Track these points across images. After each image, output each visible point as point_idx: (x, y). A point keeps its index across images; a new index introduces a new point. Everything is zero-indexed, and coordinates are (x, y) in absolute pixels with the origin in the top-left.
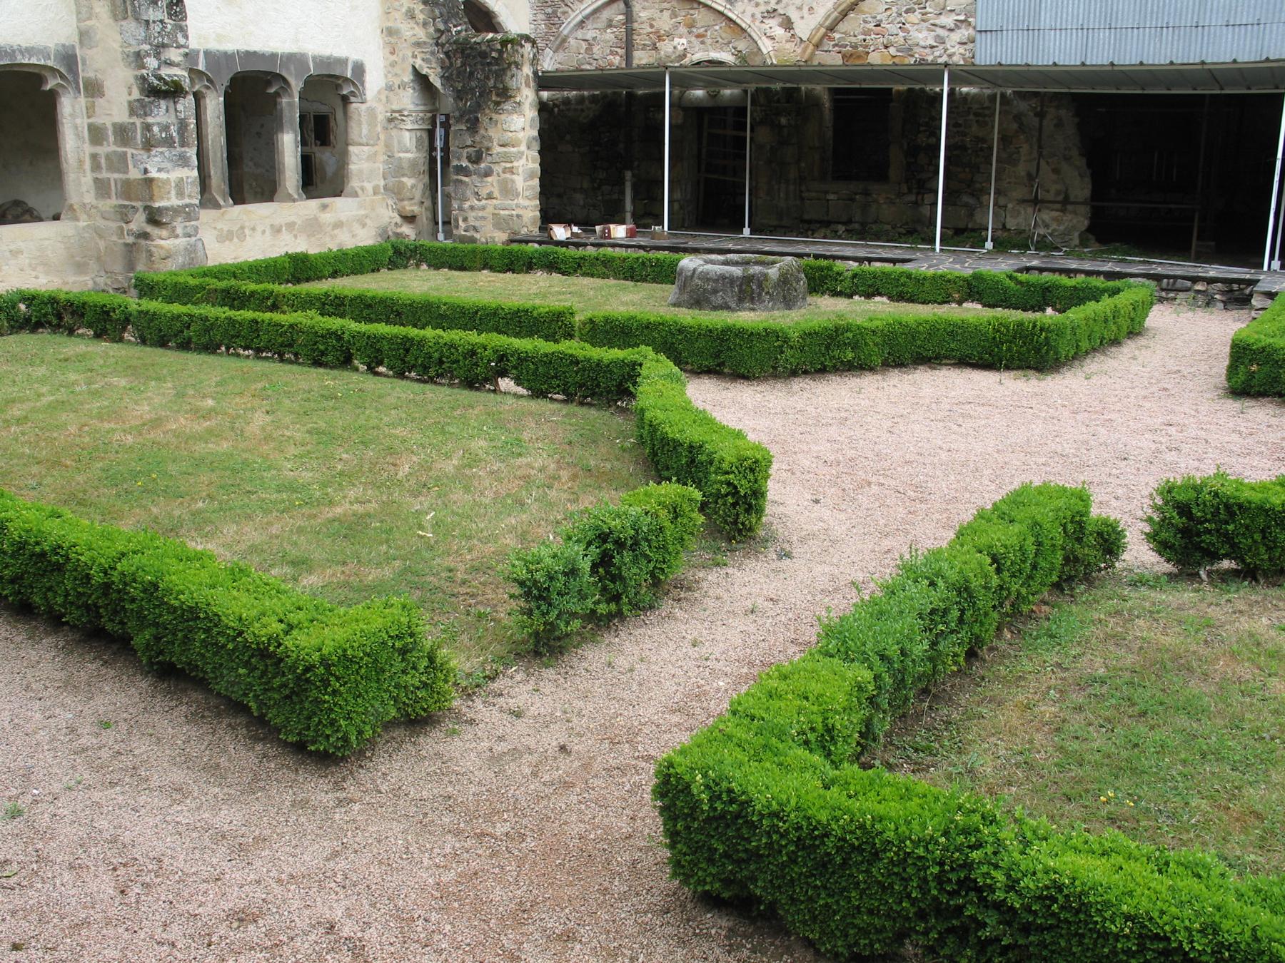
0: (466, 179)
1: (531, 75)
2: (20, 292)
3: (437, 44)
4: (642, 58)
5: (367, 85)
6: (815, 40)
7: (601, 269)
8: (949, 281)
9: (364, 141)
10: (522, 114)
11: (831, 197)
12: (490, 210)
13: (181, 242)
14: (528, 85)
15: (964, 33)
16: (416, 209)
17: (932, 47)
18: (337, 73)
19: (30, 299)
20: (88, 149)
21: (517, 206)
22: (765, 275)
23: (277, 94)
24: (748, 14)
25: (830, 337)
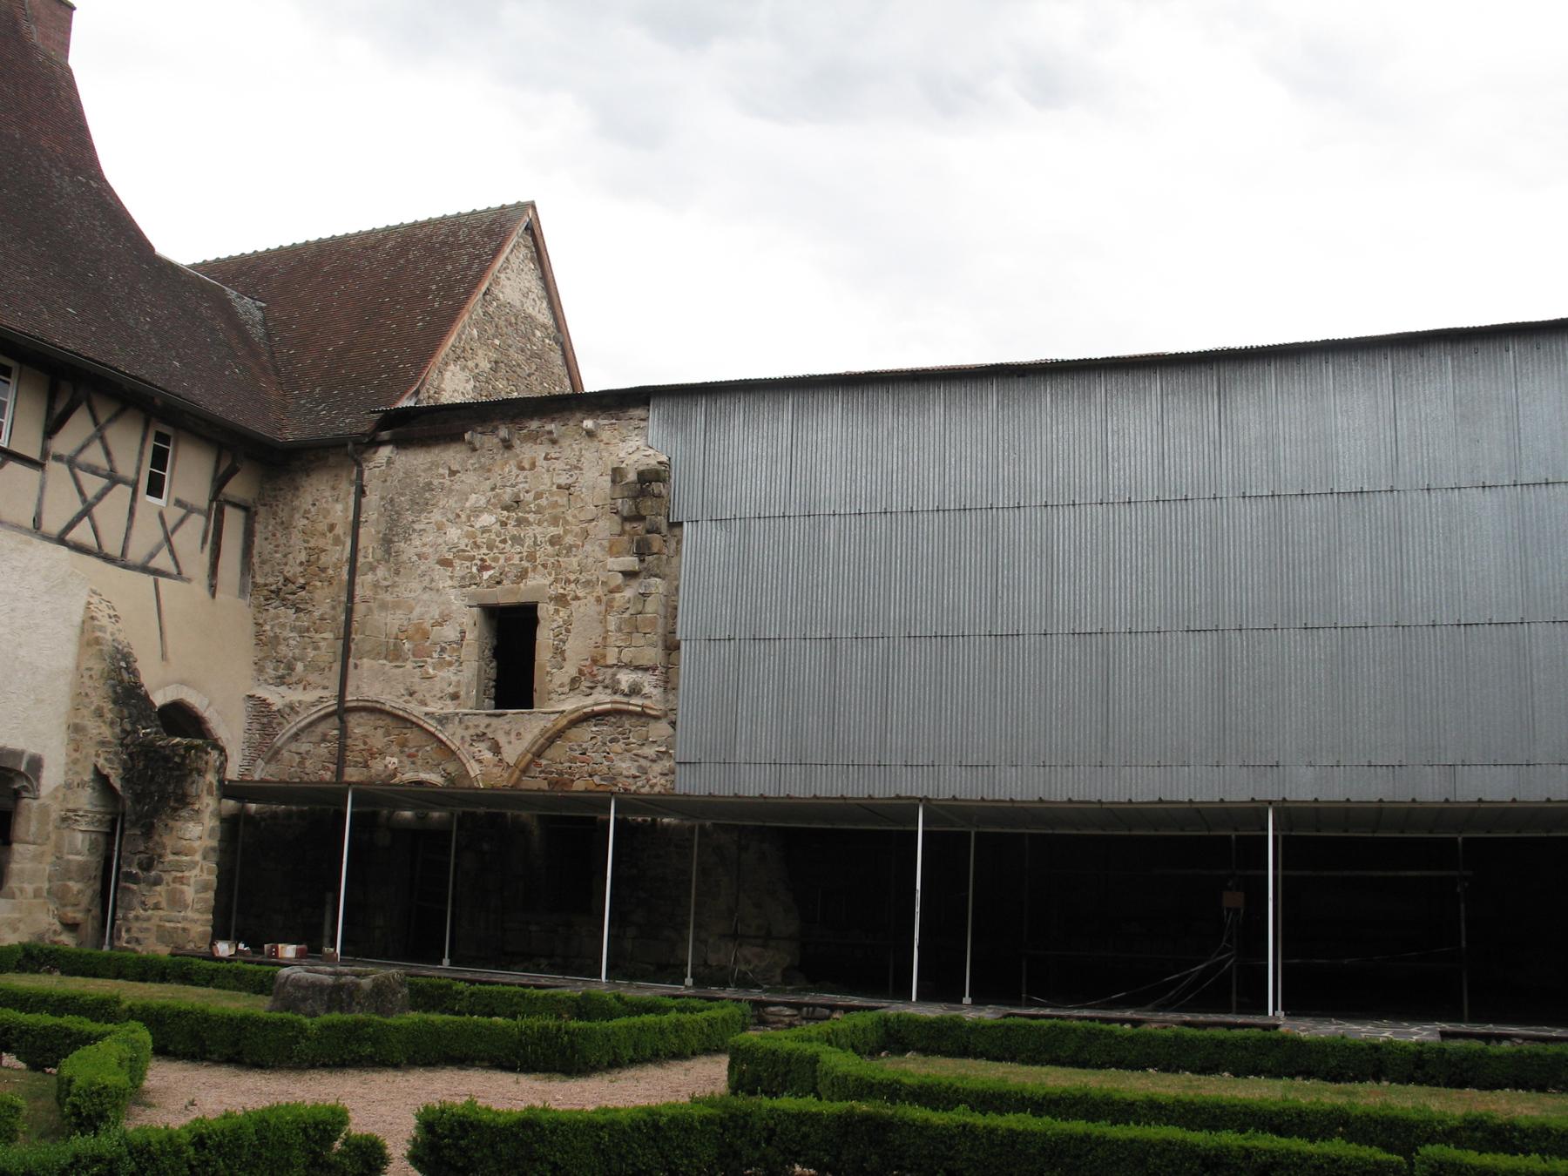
0: (134, 887)
1: (215, 783)
3: (122, 745)
4: (353, 774)
5: (43, 781)
6: (523, 764)
8: (559, 1001)
9: (31, 839)
10: (200, 822)
11: (533, 928)
12: (155, 921)
14: (210, 793)
15: (666, 764)
16: (79, 916)
17: (635, 777)
18: (9, 765)
21: (185, 919)
22: (357, 985)
24: (458, 736)
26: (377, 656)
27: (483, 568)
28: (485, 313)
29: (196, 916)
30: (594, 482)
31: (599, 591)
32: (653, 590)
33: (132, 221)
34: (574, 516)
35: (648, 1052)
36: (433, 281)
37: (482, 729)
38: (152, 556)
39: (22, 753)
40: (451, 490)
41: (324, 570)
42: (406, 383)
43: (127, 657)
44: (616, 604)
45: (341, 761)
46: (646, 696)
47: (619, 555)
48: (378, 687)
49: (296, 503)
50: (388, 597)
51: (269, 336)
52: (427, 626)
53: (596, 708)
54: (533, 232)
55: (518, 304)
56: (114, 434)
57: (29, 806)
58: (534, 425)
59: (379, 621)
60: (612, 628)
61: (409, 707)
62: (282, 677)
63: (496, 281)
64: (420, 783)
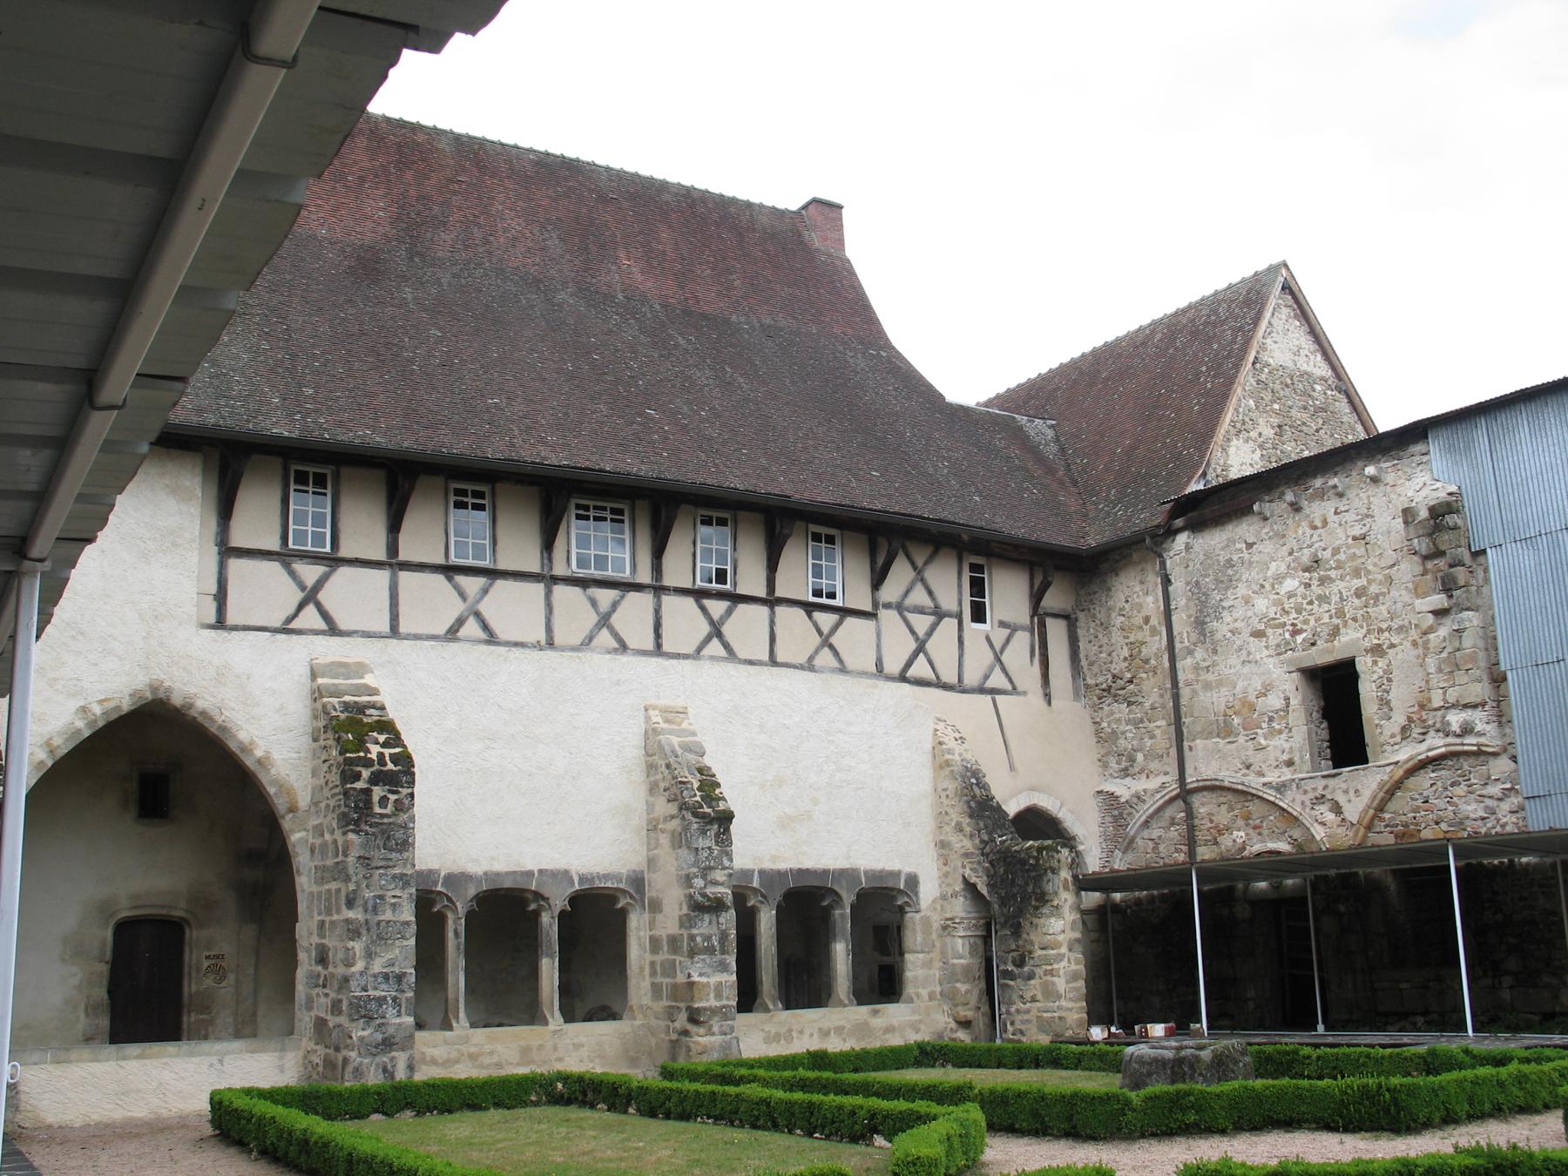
2: (559, 1072)
4: (1205, 853)
5: (921, 895)
7: (1098, 1064)
10: (1060, 916)
11: (1404, 986)
12: (1034, 1012)
13: (717, 1039)
14: (1066, 888)
15: (1515, 800)
16: (970, 1014)
17: (1483, 819)
18: (890, 885)
19: (565, 1078)
20: (648, 957)
21: (1060, 1008)
22: (1197, 1057)
23: (830, 907)
25: (1172, 1101)
26: (1209, 735)
27: (1295, 633)
28: (1259, 382)
29: (1070, 1005)
30: (1388, 528)
31: (1414, 634)
32: (1467, 624)
33: (921, 378)
34: (1375, 565)
35: (1487, 1106)
36: (1202, 363)
37: (1320, 791)
38: (986, 677)
39: (899, 872)
40: (1251, 563)
41: (1147, 661)
42: (1191, 467)
43: (976, 773)
44: (1431, 645)
45: (1192, 843)
46: (1480, 734)
47: (1425, 595)
48: (1215, 765)
49: (1111, 603)
50: (1210, 677)
51: (1062, 450)
52: (1252, 698)
53: (1431, 754)
54: (1289, 289)
55: (1290, 365)
56: (931, 574)
57: (913, 919)
58: (1318, 482)
59: (1206, 702)
60: (1432, 670)
61: (1246, 780)
62: (1126, 769)
63: (1263, 347)
64: (1270, 852)
